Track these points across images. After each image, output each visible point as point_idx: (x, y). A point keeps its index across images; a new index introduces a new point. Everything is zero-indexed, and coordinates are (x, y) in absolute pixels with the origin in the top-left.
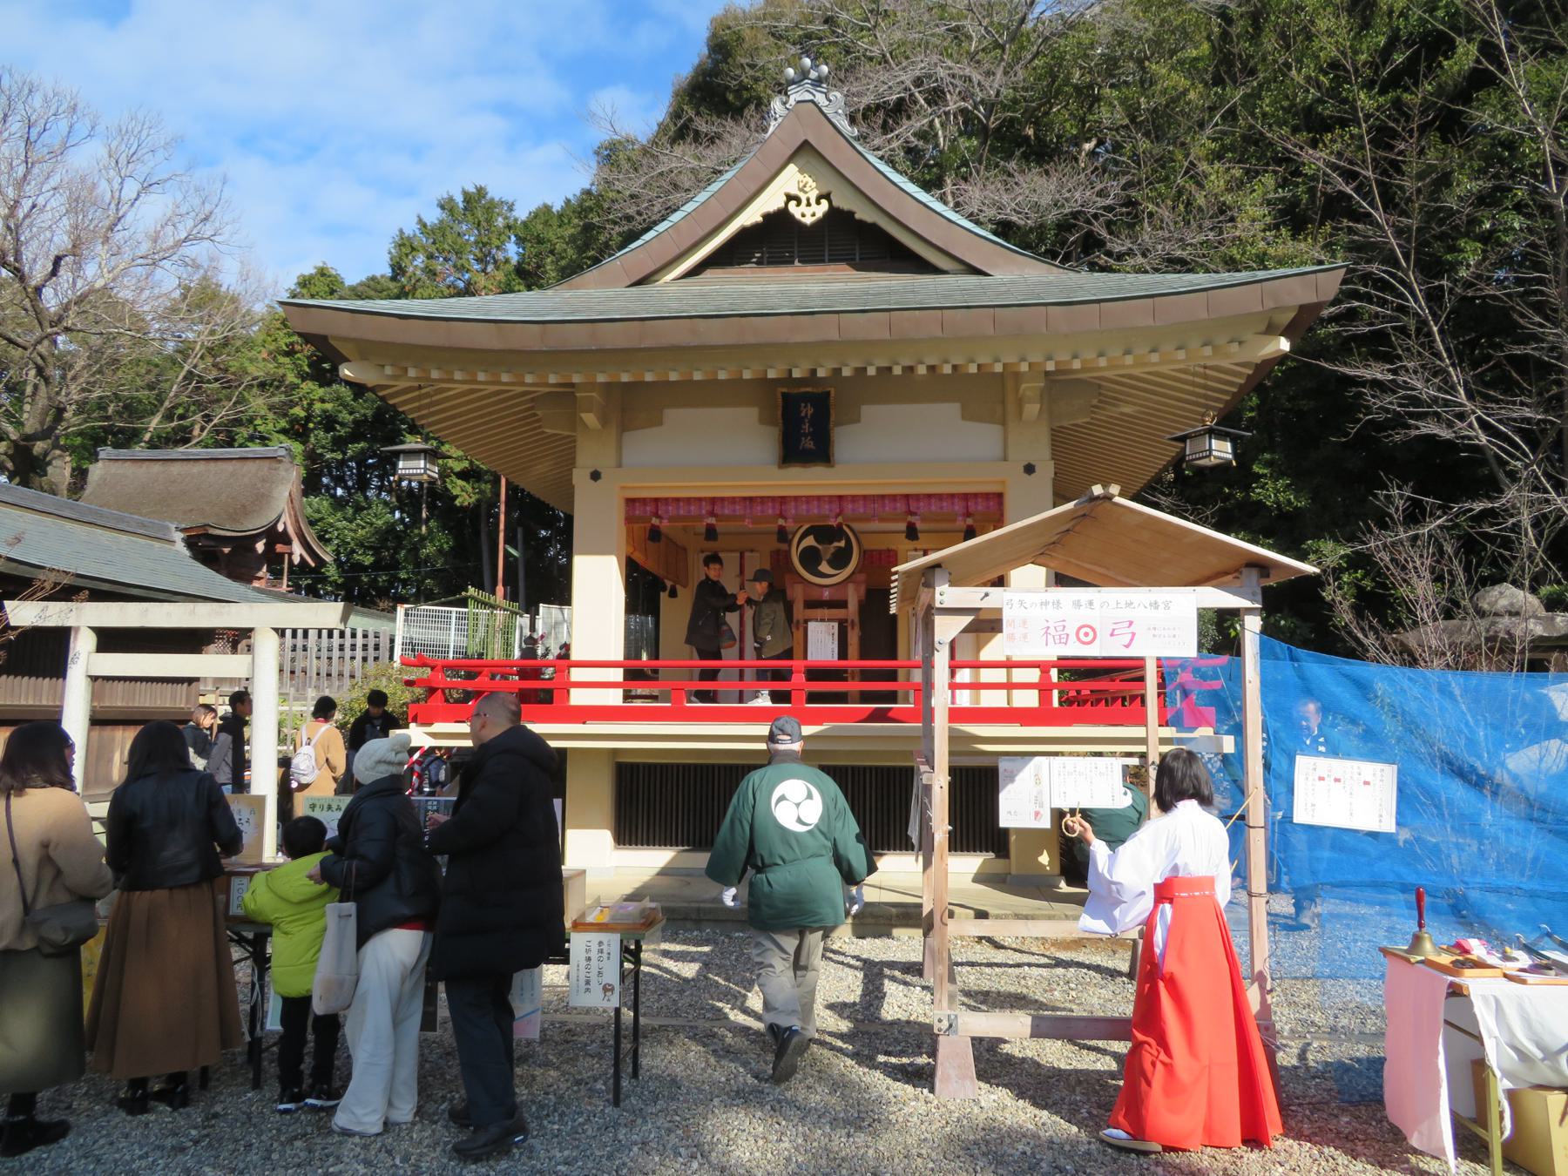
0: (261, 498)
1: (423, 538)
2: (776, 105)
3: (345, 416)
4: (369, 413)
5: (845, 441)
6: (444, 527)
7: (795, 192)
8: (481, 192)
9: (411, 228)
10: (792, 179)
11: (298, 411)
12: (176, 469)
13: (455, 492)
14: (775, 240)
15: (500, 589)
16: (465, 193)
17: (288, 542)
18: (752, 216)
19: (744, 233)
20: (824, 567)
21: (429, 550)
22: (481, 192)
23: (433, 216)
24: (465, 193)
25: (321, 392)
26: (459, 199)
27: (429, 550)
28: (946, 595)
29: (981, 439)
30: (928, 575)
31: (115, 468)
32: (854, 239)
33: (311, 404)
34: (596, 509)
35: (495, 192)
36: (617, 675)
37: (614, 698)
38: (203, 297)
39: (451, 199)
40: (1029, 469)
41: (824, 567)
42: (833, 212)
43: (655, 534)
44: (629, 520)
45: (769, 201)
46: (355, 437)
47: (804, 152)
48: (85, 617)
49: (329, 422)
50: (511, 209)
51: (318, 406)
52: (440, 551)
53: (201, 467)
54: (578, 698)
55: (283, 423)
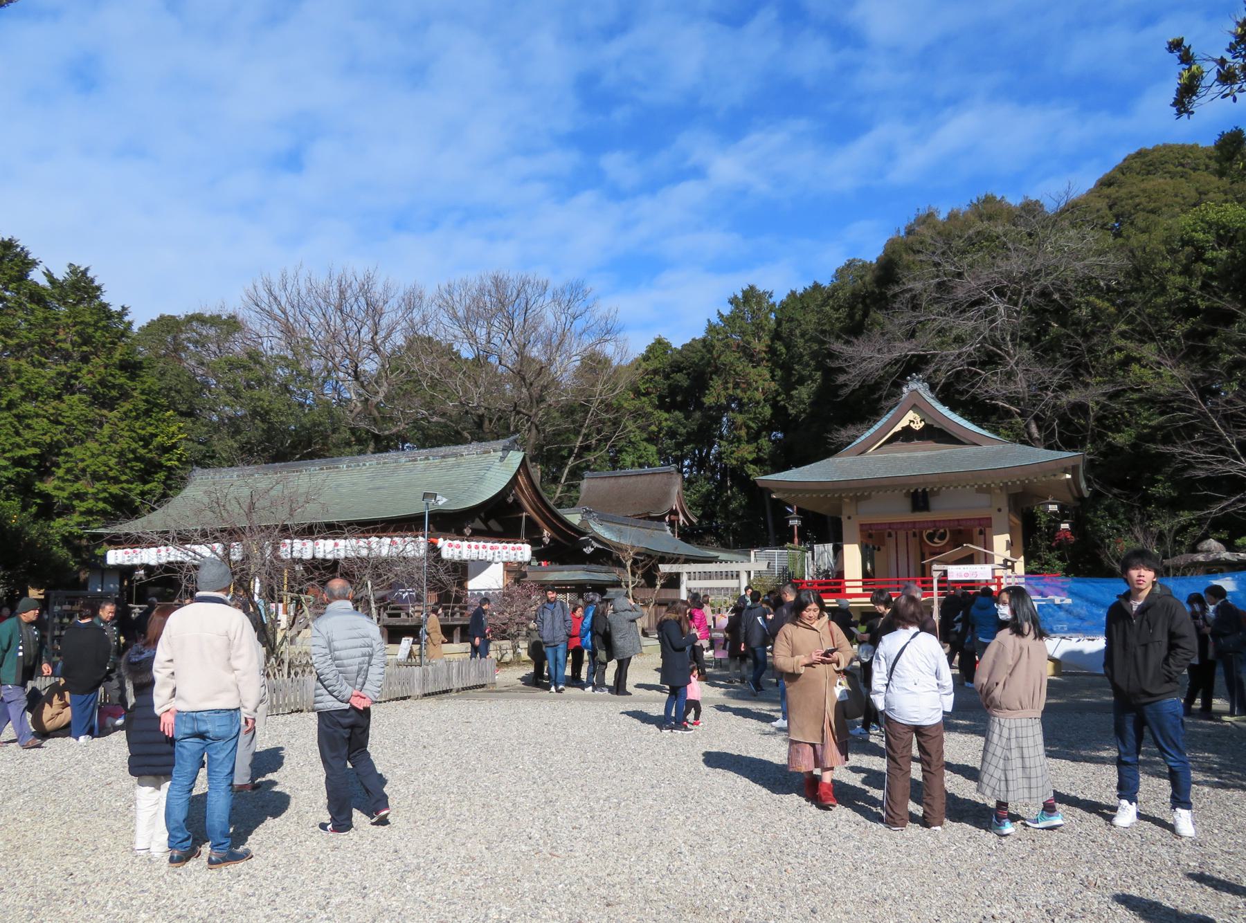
0: (666, 495)
1: (729, 499)
2: (905, 389)
3: (682, 430)
4: (696, 427)
5: (934, 503)
6: (741, 491)
7: (912, 420)
8: (752, 288)
9: (715, 320)
10: (911, 415)
11: (653, 428)
12: (622, 480)
13: (750, 472)
14: (907, 435)
15: (796, 540)
16: (743, 292)
17: (677, 514)
18: (898, 428)
19: (895, 434)
20: (936, 540)
21: (734, 505)
22: (752, 288)
23: (727, 310)
24: (743, 292)
25: (666, 415)
26: (740, 295)
27: (734, 505)
28: (935, 567)
29: (983, 499)
30: (932, 563)
31: (593, 482)
32: (934, 433)
33: (660, 423)
34: (849, 528)
35: (761, 288)
36: (860, 584)
37: (860, 591)
38: (594, 364)
39: (736, 297)
40: (999, 510)
41: (936, 540)
42: (926, 425)
43: (870, 536)
44: (861, 531)
45: (904, 423)
46: (687, 442)
47: (914, 407)
48: (684, 569)
49: (672, 434)
50: (770, 296)
51: (664, 424)
52: (741, 506)
53: (634, 479)
54: (848, 591)
55: (645, 436)
